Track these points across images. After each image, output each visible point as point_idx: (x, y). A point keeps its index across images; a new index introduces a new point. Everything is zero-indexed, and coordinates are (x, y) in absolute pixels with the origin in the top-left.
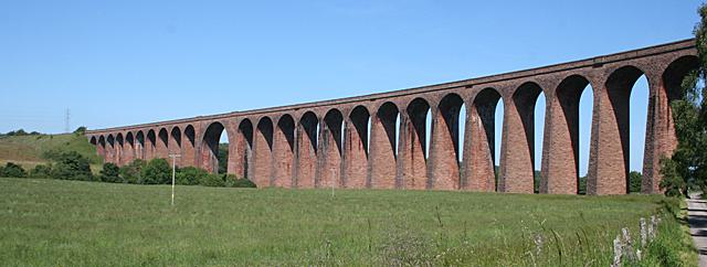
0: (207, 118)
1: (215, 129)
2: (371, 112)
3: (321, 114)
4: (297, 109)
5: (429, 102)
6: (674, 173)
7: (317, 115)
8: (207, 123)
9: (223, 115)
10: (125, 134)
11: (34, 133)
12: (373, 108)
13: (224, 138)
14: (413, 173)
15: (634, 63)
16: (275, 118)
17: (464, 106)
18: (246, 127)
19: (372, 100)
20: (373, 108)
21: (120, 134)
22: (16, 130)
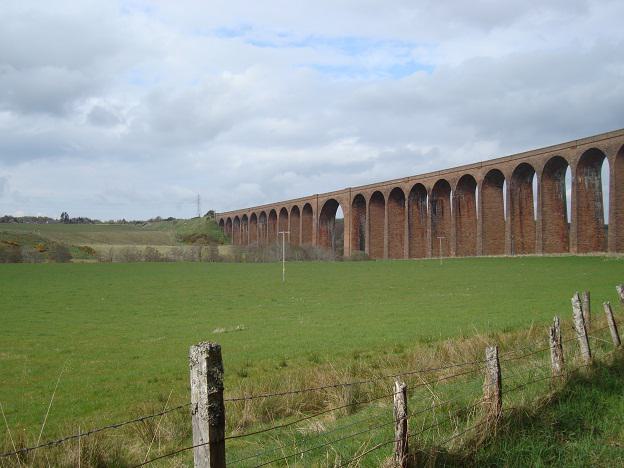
0: (323, 195)
1: (331, 205)
2: (536, 170)
3: (407, 188)
4: (573, 147)
5: (535, 166)
6: (554, 392)
7: (426, 186)
8: (323, 201)
9: (338, 192)
10: (249, 215)
11: (170, 219)
12: (479, 176)
13: (340, 214)
14: (523, 236)
15: (600, 145)
16: (233, 217)
17: (569, 168)
18: (359, 200)
19: (478, 168)
20: (479, 176)
21: (245, 215)
22: (154, 217)
